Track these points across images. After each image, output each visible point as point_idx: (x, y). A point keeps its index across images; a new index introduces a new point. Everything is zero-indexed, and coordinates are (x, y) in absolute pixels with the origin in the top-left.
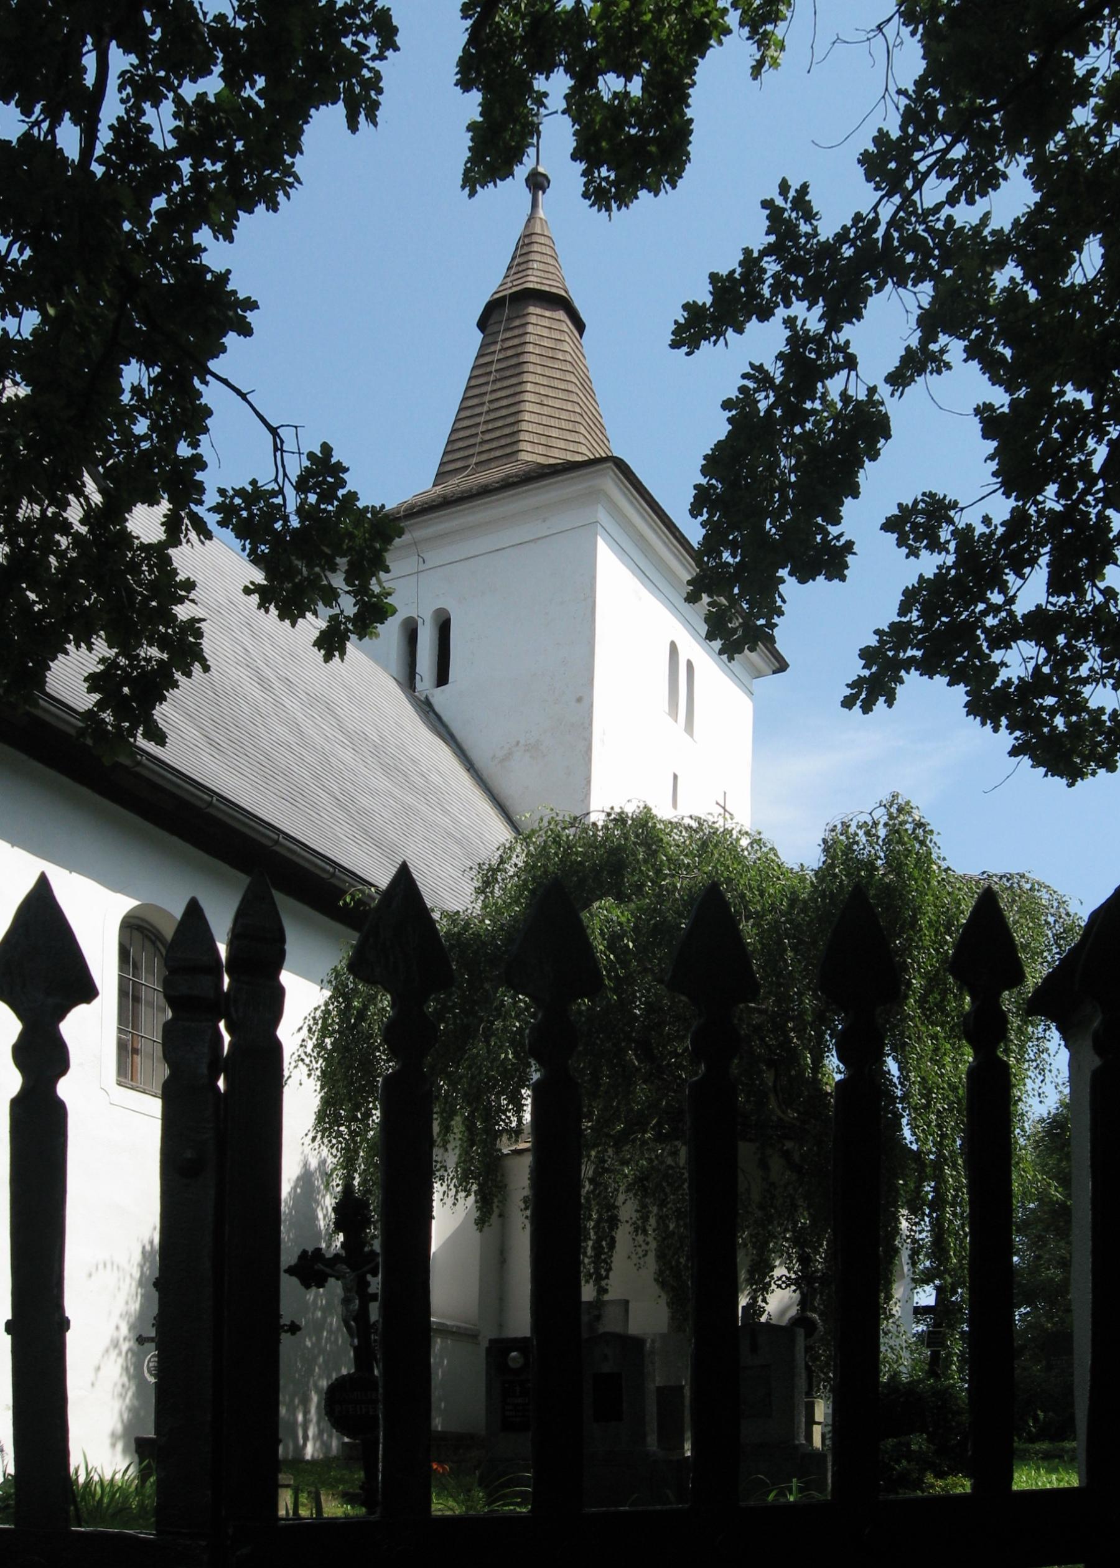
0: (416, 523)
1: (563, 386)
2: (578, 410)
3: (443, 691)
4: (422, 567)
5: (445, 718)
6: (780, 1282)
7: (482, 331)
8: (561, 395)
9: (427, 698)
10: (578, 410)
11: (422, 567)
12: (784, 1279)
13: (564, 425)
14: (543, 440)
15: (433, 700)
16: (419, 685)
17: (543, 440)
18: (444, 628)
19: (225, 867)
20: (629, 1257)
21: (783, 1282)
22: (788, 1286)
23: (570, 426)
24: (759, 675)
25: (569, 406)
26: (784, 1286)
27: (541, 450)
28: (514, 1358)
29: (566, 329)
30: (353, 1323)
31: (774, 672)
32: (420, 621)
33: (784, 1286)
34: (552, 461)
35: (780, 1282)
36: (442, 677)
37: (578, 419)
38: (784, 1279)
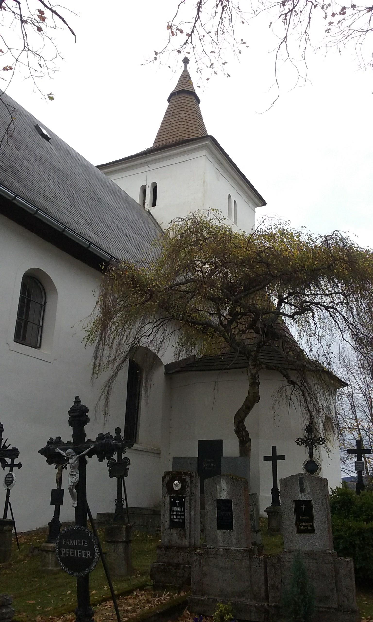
0: (146, 156)
1: (194, 117)
2: (198, 124)
3: (154, 208)
4: (148, 169)
5: (154, 217)
6: (298, 442)
7: (169, 102)
8: (193, 120)
9: (149, 211)
10: (198, 124)
11: (148, 169)
12: (300, 440)
13: (194, 128)
14: (188, 133)
15: (150, 211)
16: (146, 206)
17: (188, 133)
18: (155, 188)
19: (68, 256)
20: (290, 221)
21: (300, 441)
22: (302, 444)
23: (196, 129)
24: (258, 206)
25: (196, 123)
26: (300, 443)
27: (186, 135)
28: (176, 485)
29: (194, 101)
30: (74, 490)
31: (262, 206)
32: (147, 186)
33: (300, 443)
34: (188, 138)
35: (298, 442)
36: (154, 204)
37: (198, 127)
38: (300, 440)
